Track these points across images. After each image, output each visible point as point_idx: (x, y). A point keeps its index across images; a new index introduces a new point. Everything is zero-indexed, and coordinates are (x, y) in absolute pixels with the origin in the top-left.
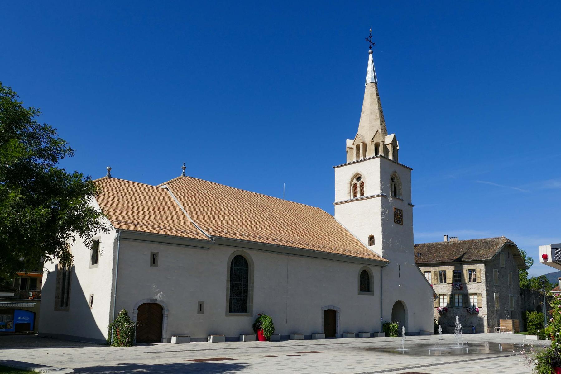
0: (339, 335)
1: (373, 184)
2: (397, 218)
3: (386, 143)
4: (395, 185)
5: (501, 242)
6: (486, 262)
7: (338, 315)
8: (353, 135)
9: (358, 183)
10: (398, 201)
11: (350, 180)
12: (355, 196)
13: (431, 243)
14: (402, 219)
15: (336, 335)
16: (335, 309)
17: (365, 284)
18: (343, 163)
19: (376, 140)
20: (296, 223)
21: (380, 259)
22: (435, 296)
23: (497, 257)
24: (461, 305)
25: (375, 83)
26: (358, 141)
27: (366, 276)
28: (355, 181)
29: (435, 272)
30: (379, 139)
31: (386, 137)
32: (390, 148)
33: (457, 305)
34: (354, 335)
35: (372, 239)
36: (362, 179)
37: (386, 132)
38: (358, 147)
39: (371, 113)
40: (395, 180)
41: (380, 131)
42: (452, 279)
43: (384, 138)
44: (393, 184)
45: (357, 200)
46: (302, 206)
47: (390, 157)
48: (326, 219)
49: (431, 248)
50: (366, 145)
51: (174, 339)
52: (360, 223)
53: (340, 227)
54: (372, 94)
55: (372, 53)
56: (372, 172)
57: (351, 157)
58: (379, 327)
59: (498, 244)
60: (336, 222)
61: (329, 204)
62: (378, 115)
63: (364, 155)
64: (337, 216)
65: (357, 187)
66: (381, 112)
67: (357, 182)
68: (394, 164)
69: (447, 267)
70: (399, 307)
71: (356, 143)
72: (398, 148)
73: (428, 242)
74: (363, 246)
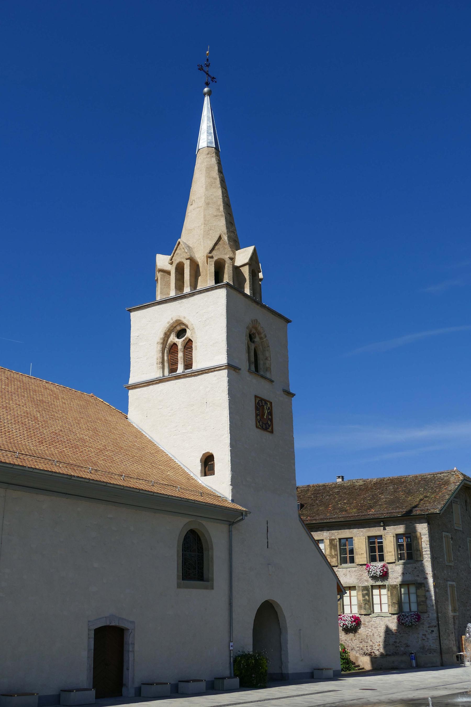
0: (132, 692)
1: (212, 343)
2: (260, 416)
3: (238, 263)
4: (253, 355)
5: (452, 479)
6: (428, 518)
7: (128, 639)
8: (169, 247)
9: (180, 342)
10: (263, 382)
11: (162, 336)
12: (173, 369)
13: (321, 483)
14: (271, 420)
15: (124, 690)
16: (122, 625)
17: (194, 563)
18: (147, 300)
19: (217, 255)
20: (36, 418)
21: (226, 505)
22: (341, 590)
23: (448, 508)
24: (385, 608)
25: (217, 148)
26: (180, 256)
27: (196, 540)
28: (173, 338)
29: (331, 541)
30: (224, 253)
31: (237, 252)
32: (246, 271)
33: (377, 609)
34: (203, 685)
35: (208, 463)
36: (188, 334)
37: (236, 245)
38: (180, 269)
39: (208, 204)
40: (257, 339)
41: (225, 238)
42: (365, 555)
43: (234, 254)
44: (252, 346)
45: (178, 377)
46: (55, 388)
47: (247, 291)
48: (110, 418)
49: (320, 493)
50: (198, 266)
51: (16, 696)
52: (182, 424)
53: (138, 435)
54: (209, 169)
55: (209, 93)
56: (208, 319)
57: (165, 288)
58: (223, 666)
59: (447, 483)
60: (130, 425)
61: (114, 385)
62: (222, 208)
63: (194, 284)
64: (135, 415)
65: (177, 352)
66: (227, 205)
67: (176, 340)
68: (254, 305)
69: (355, 531)
70: (268, 614)
71: (177, 260)
72: (261, 275)
73: (315, 483)
74: (189, 478)
